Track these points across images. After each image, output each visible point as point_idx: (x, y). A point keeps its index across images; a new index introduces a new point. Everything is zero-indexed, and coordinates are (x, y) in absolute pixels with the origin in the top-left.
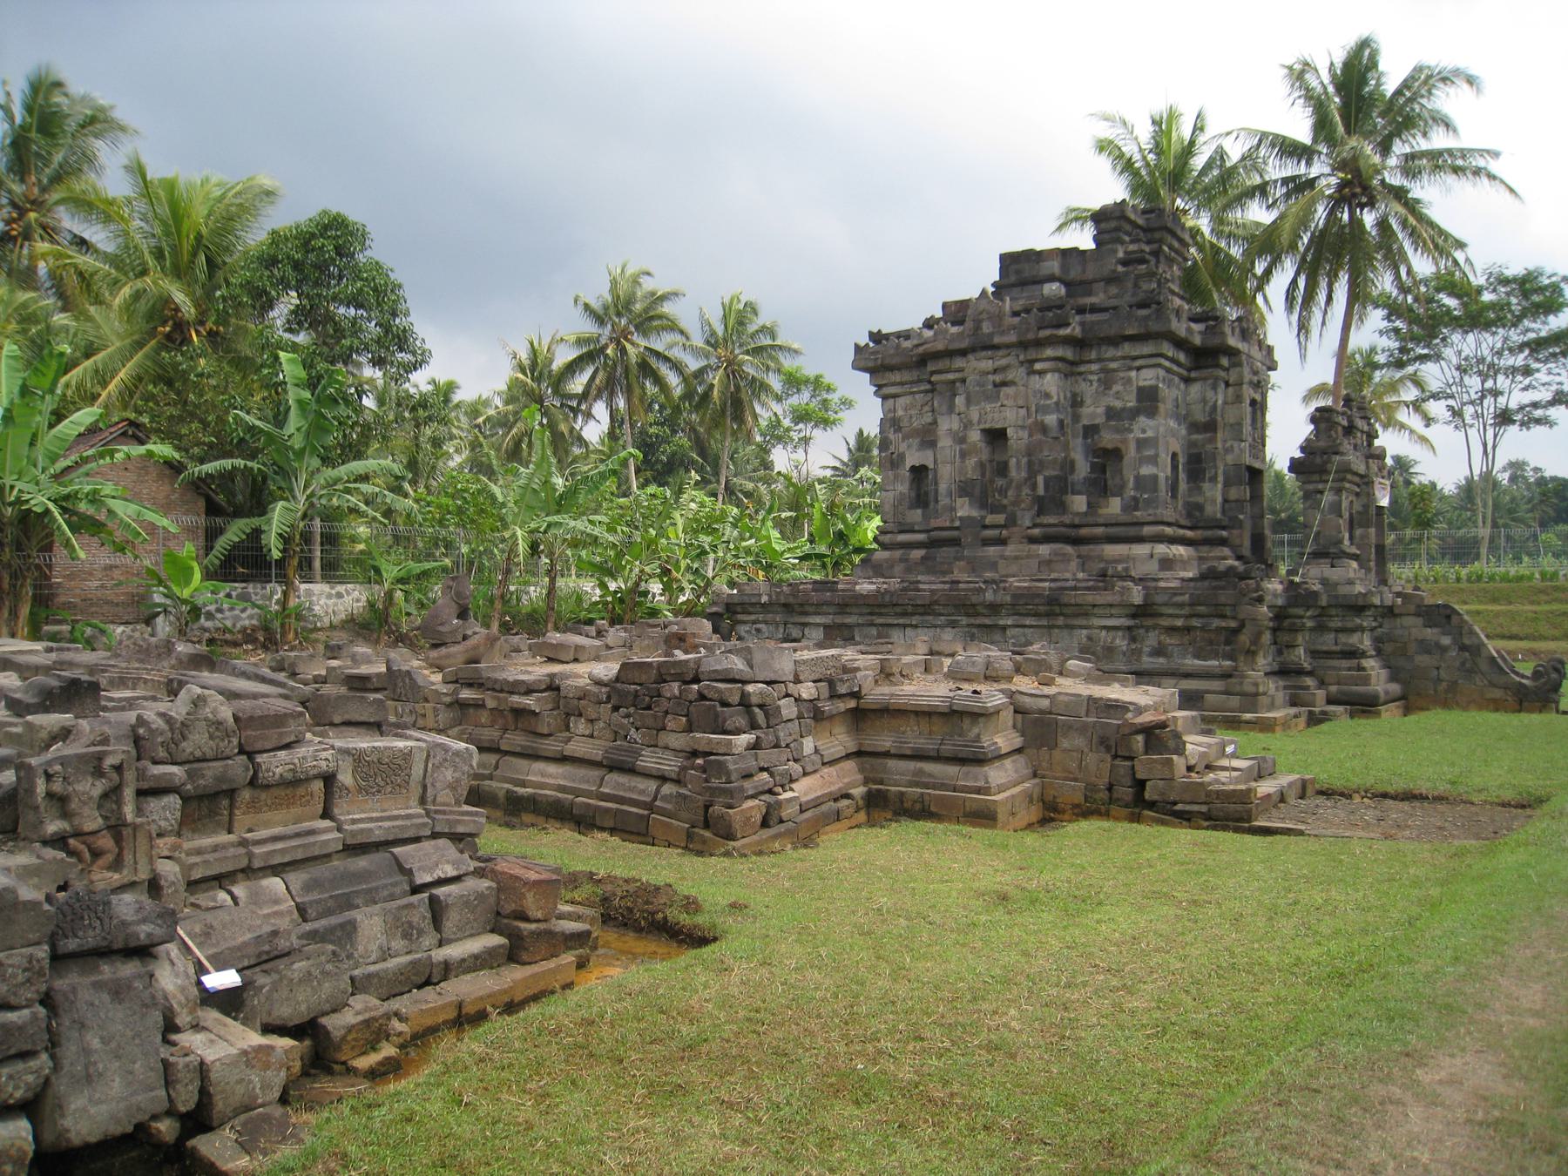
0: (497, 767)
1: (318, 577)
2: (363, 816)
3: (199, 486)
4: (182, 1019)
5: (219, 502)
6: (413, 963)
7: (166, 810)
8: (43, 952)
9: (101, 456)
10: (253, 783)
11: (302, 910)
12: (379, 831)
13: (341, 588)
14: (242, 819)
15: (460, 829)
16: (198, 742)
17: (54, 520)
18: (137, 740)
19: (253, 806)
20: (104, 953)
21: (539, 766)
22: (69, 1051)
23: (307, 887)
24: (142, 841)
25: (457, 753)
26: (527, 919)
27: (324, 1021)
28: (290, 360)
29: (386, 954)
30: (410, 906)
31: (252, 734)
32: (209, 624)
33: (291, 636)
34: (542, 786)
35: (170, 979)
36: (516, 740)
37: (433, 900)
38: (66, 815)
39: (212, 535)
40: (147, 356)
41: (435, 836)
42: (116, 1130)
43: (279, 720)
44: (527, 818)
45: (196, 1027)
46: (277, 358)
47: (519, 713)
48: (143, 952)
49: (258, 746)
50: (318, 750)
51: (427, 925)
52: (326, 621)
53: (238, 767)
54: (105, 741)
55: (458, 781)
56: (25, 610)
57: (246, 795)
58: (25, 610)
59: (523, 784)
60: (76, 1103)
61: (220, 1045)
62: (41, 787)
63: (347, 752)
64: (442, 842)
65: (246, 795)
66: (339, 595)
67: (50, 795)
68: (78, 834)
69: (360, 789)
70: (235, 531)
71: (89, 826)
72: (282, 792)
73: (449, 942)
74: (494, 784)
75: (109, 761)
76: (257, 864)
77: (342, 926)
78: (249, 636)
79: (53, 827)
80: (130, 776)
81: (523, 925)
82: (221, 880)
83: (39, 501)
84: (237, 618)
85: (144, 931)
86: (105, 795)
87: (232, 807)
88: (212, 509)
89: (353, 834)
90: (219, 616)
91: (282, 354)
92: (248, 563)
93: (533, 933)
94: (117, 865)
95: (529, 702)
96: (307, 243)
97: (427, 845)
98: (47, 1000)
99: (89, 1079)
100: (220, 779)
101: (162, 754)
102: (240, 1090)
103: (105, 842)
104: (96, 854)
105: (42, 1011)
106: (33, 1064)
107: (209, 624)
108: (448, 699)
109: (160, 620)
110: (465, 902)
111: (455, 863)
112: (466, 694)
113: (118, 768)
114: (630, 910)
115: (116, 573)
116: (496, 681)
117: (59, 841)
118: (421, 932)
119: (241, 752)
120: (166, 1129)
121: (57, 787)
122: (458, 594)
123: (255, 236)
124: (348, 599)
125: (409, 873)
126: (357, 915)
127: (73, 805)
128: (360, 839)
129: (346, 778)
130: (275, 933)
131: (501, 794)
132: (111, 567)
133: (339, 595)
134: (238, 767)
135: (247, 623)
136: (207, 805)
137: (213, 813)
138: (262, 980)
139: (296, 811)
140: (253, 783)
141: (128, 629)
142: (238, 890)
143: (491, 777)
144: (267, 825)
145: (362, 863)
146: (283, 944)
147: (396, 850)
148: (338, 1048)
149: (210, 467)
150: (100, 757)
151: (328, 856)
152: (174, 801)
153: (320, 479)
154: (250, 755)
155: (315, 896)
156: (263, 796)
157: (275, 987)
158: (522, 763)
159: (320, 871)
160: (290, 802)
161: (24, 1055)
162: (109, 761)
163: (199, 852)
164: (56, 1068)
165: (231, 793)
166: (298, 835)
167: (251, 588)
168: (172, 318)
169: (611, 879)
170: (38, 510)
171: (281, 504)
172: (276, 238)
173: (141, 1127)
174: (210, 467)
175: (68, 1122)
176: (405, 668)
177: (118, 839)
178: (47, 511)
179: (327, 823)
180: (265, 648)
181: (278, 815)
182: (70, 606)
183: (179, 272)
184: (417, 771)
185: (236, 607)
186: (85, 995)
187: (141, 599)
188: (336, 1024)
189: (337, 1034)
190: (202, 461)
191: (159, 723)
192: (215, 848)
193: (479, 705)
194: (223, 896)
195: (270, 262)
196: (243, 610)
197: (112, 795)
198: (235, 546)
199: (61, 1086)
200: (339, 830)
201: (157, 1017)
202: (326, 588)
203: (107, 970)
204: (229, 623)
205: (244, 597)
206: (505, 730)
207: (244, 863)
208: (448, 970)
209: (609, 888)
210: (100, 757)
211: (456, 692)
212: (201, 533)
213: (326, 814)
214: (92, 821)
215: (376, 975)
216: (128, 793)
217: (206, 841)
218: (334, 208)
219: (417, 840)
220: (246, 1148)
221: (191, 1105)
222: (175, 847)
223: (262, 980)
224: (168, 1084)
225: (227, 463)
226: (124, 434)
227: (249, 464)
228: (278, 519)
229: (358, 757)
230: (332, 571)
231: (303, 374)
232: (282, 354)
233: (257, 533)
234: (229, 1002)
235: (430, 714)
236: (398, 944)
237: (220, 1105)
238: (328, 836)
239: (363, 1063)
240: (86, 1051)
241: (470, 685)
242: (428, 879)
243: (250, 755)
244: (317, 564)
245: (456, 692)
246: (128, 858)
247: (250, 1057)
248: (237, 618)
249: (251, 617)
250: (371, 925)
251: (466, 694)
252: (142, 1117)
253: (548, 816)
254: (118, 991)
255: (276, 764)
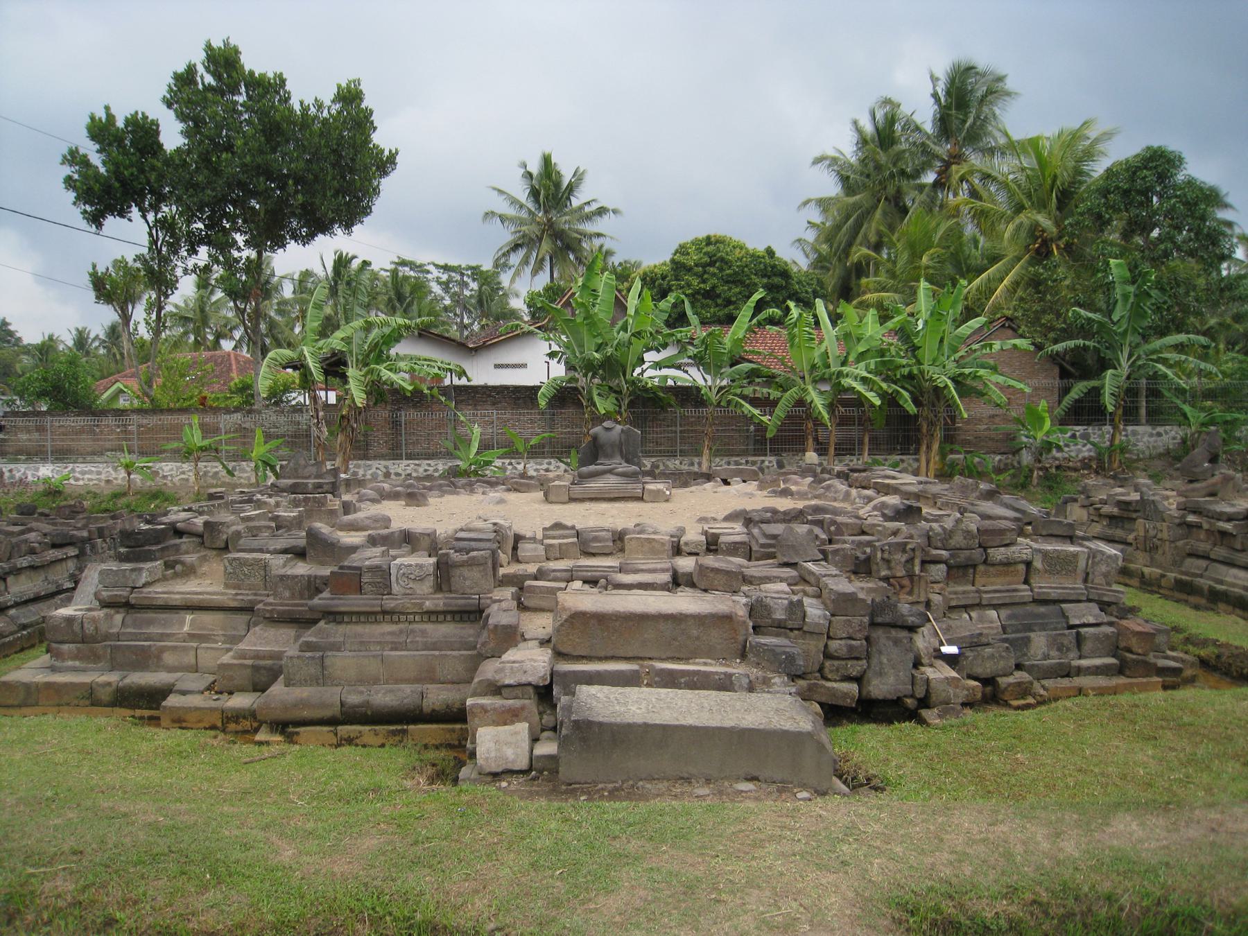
0: (1206, 569)
1: (1144, 421)
2: (1045, 585)
3: (1054, 358)
4: (925, 660)
5: (1073, 368)
6: (1060, 664)
7: (939, 571)
8: (866, 619)
9: (984, 347)
10: (985, 562)
11: (1004, 628)
12: (1054, 594)
13: (1160, 429)
14: (980, 580)
15: (1106, 599)
16: (958, 540)
17: (950, 392)
18: (929, 538)
19: (986, 573)
20: (894, 626)
21: (1234, 571)
22: (874, 661)
23: (1009, 617)
24: (923, 583)
25: (1109, 557)
26: (1130, 651)
27: (999, 679)
28: (1117, 265)
29: (1046, 657)
30: (1064, 635)
31: (988, 537)
32: (1059, 455)
33: (1116, 465)
34: (1234, 585)
35: (922, 641)
36: (1220, 552)
37: (1078, 634)
38: (889, 568)
39: (1065, 391)
40: (1022, 267)
41: (1089, 600)
42: (890, 697)
43: (1002, 532)
44: (1222, 606)
45: (931, 666)
46: (1108, 264)
47: (1224, 534)
48: (912, 629)
49: (989, 544)
50: (1024, 547)
51: (1073, 645)
52: (1147, 453)
53: (977, 554)
54: (911, 537)
55: (1109, 572)
56: (936, 446)
57: (981, 568)
58: (936, 446)
59: (1221, 582)
60: (875, 682)
61: (938, 673)
62: (879, 555)
63: (1039, 551)
64: (1091, 604)
65: (981, 568)
66: (1159, 435)
67: (883, 559)
68: (894, 577)
69: (1046, 571)
70: (1079, 389)
71: (899, 574)
72: (1001, 568)
73: (1085, 657)
74: (1202, 581)
75: (909, 546)
76: (984, 602)
77: (1022, 638)
78: (1085, 464)
79: (883, 573)
80: (918, 553)
81: (1128, 655)
82: (966, 608)
83: (943, 380)
84: (1079, 451)
85: (911, 620)
86: (907, 561)
87: (974, 573)
88: (1064, 374)
89: (1039, 594)
90: (1066, 449)
91: (1112, 261)
92: (1087, 412)
93: (1134, 660)
94: (910, 593)
95: (1228, 526)
96: (1134, 173)
97: (1082, 605)
98: (867, 639)
99: (881, 674)
100: (969, 558)
101: (939, 545)
102: (944, 694)
103: (906, 582)
104: (902, 587)
105: (864, 642)
106: (860, 663)
107: (1059, 455)
108: (1177, 521)
109: (1024, 451)
110: (1096, 637)
111: (1095, 616)
112: (1191, 518)
113: (913, 550)
114: (1230, 665)
115: (997, 420)
116: (1209, 511)
117: (886, 579)
118: (1068, 650)
119: (980, 546)
120: (910, 702)
121: (886, 556)
122: (1210, 445)
123: (1098, 168)
124: (1165, 437)
125: (1067, 617)
126: (1032, 635)
127: (893, 564)
128: (1042, 597)
129: (1038, 564)
130: (981, 634)
131: (1206, 588)
132: (993, 416)
133: (1159, 435)
134: (977, 554)
135: (1086, 454)
136: (960, 570)
137: (965, 575)
138: (968, 653)
139: (1008, 579)
140: (985, 562)
141: (1003, 457)
142: (973, 614)
143: (1201, 576)
144: (992, 584)
145: (1042, 609)
146: (984, 640)
147: (1063, 606)
148: (1003, 692)
149: (1059, 347)
150: (906, 544)
151: (1025, 603)
152: (943, 567)
153: (1141, 351)
154: (985, 549)
155: (1013, 622)
156: (991, 569)
157: (975, 658)
158: (1223, 568)
159: (1018, 610)
160: (1006, 574)
161: (857, 659)
162: (909, 546)
163: (956, 593)
164: (869, 667)
165: (974, 566)
166: (1008, 591)
167: (1090, 430)
168: (1041, 236)
169: (1227, 645)
170: (942, 385)
171: (1110, 372)
172: (1110, 173)
173: (899, 698)
174: (1059, 347)
175: (871, 688)
176: (1152, 498)
177: (912, 582)
178: (946, 386)
179: (1026, 587)
180: (1097, 473)
181: (1000, 580)
182: (965, 443)
183: (1042, 205)
184: (1082, 564)
185: (1079, 444)
186: (883, 641)
187: (1010, 437)
188: (1003, 681)
189: (1003, 686)
190: (1056, 342)
191: (940, 530)
192: (964, 592)
193: (1199, 526)
194: (966, 616)
195: (1105, 192)
196: (1084, 445)
197: (910, 561)
198: (1077, 401)
199: (870, 674)
200: (1032, 590)
201: (911, 656)
202: (1148, 429)
203: (894, 633)
204: (1073, 454)
205: (1085, 436)
206: (1215, 545)
207: (977, 601)
208: (1079, 671)
209: (1223, 650)
210: (906, 544)
211: (1183, 516)
212: (1056, 391)
213: (1026, 582)
214: (901, 572)
215: (1037, 666)
216: (917, 562)
217: (960, 588)
218: (1156, 145)
219: (1079, 601)
220: (940, 716)
221: (922, 696)
222: (942, 589)
223: (968, 653)
224: (913, 684)
225: (1071, 344)
226: (1003, 326)
227: (1087, 343)
228: (1110, 383)
229: (1045, 554)
230: (1155, 417)
231: (1128, 274)
232: (1112, 261)
233: (1096, 392)
234: (951, 660)
235: (1165, 530)
236: (1054, 653)
237: (934, 698)
238: (1024, 592)
239: (1015, 703)
240: (881, 663)
241: (1194, 512)
242: (1077, 622)
243: (985, 549)
244: (1143, 411)
245: (1183, 516)
246: (916, 590)
247: (949, 681)
248: (1079, 451)
249: (1090, 450)
250: (1039, 642)
251: (1191, 518)
252: (900, 695)
253: (1234, 606)
254: (896, 642)
255: (998, 554)
